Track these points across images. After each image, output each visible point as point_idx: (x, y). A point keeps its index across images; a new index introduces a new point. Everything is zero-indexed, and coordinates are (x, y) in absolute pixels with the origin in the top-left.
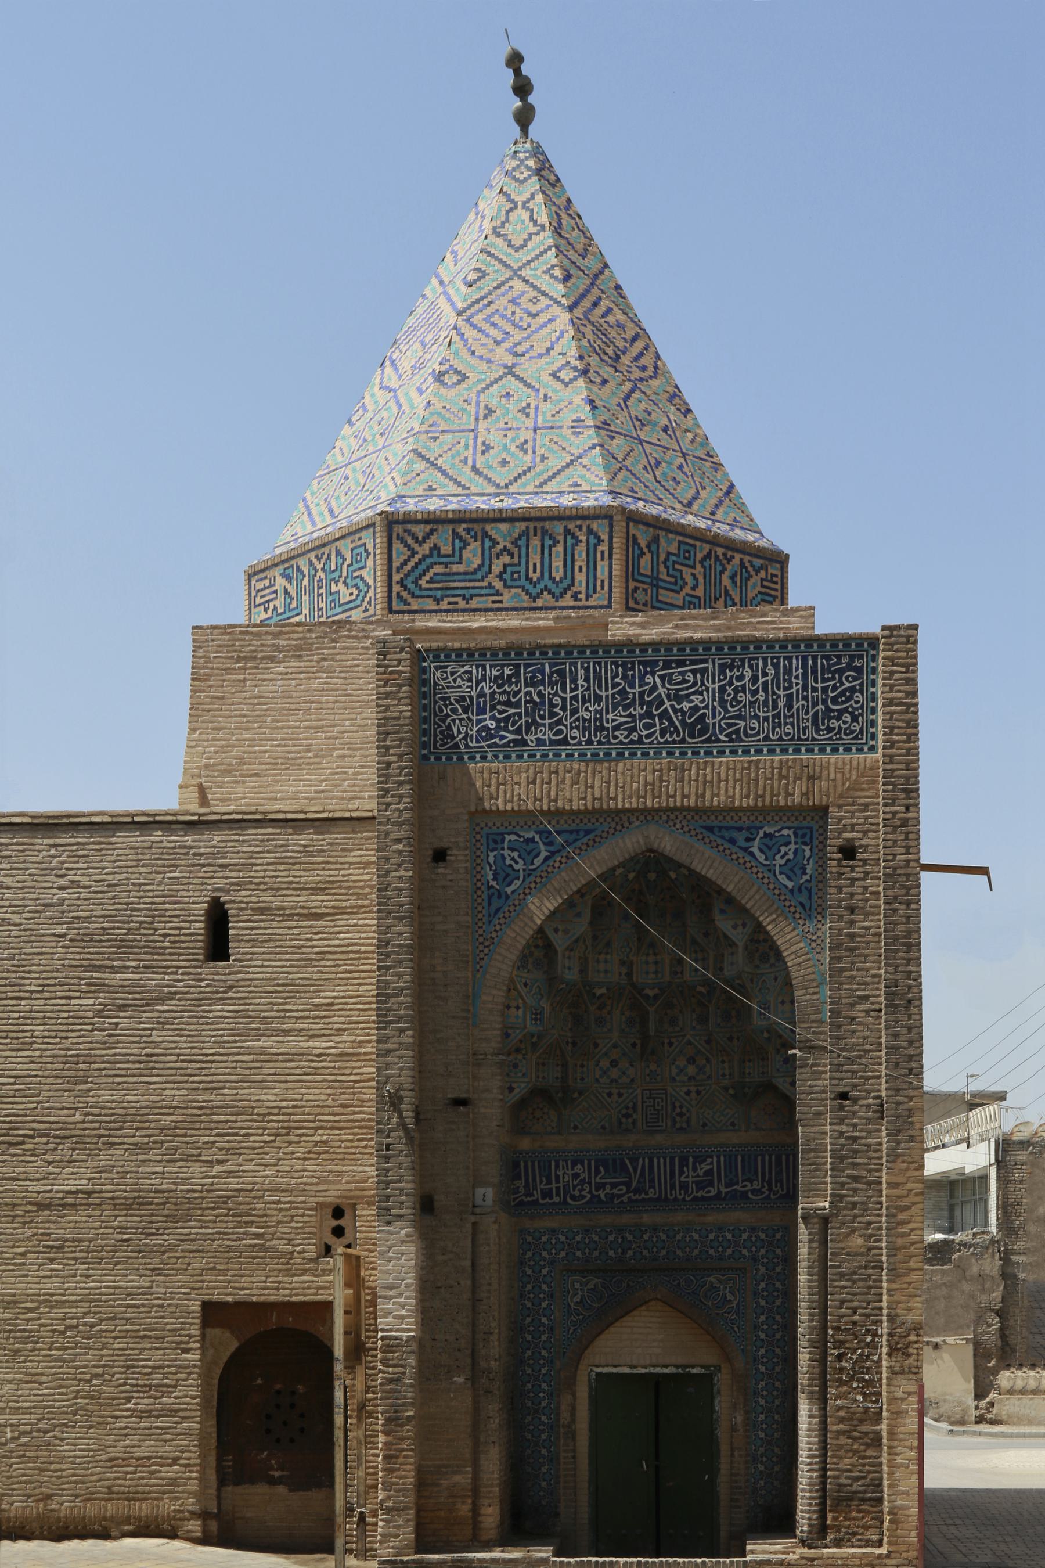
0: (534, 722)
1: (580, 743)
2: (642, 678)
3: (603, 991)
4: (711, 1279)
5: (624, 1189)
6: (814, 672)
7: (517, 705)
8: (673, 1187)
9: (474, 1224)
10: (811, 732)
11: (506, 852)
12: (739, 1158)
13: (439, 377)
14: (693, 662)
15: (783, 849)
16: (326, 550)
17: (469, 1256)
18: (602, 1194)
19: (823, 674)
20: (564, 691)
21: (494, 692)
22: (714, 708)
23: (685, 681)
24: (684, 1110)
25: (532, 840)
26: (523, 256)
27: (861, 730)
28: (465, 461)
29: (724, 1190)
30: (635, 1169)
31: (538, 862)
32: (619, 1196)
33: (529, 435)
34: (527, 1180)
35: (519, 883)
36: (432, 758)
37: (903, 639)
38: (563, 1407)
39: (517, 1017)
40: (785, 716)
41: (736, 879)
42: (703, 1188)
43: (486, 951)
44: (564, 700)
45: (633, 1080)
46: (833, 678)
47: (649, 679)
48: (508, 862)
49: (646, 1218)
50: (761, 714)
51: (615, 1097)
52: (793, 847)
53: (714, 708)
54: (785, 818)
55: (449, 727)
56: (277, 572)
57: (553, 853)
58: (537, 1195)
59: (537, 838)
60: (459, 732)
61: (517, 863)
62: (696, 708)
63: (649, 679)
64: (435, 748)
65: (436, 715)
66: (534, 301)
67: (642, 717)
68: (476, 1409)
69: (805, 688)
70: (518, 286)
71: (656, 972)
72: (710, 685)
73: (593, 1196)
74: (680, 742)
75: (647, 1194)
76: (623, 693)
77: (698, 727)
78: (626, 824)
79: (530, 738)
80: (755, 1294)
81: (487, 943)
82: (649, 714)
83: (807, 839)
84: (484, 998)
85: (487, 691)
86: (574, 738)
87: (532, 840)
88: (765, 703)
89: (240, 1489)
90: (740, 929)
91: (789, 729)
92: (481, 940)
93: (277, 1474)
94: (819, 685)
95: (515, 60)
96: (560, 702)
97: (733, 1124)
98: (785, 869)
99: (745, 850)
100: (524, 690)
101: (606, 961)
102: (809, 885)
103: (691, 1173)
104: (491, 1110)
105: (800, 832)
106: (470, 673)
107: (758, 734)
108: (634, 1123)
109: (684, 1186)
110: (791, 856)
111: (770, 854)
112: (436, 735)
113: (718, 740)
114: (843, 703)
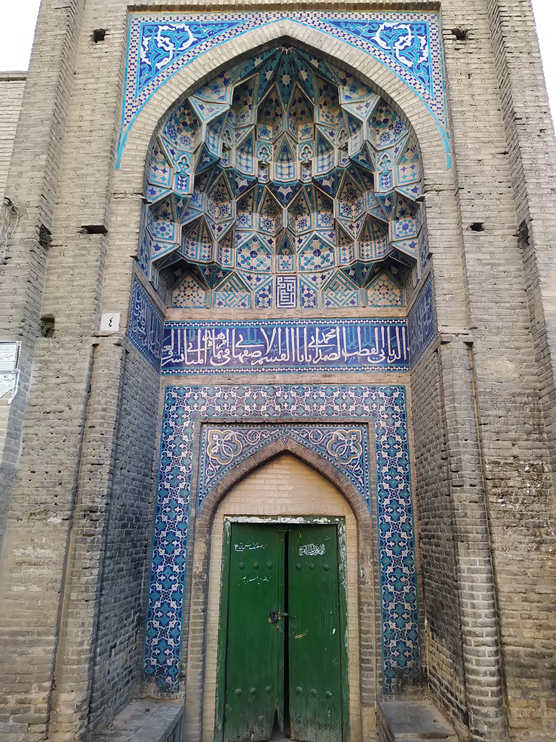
4: (337, 433)
5: (260, 353)
8: (302, 352)
9: (95, 346)
12: (359, 329)
15: (402, 39)
17: (85, 379)
18: (241, 358)
24: (311, 292)
25: (183, 30)
29: (346, 355)
30: (270, 337)
31: (186, 45)
34: (176, 345)
35: (168, 60)
38: (196, 556)
39: (164, 179)
41: (362, 59)
42: (328, 354)
43: (134, 110)
45: (269, 268)
48: (160, 44)
51: (254, 281)
52: (410, 37)
54: (402, 17)
57: (200, 39)
59: (187, 28)
61: (167, 45)
71: (289, 174)
73: (233, 359)
78: (265, 20)
80: (378, 446)
81: (135, 104)
84: (128, 146)
87: (183, 30)
90: (364, 109)
92: (130, 101)
97: (353, 302)
98: (406, 53)
99: (369, 38)
101: (247, 160)
102: (427, 65)
103: (318, 341)
108: (269, 302)
109: (312, 352)
110: (409, 43)
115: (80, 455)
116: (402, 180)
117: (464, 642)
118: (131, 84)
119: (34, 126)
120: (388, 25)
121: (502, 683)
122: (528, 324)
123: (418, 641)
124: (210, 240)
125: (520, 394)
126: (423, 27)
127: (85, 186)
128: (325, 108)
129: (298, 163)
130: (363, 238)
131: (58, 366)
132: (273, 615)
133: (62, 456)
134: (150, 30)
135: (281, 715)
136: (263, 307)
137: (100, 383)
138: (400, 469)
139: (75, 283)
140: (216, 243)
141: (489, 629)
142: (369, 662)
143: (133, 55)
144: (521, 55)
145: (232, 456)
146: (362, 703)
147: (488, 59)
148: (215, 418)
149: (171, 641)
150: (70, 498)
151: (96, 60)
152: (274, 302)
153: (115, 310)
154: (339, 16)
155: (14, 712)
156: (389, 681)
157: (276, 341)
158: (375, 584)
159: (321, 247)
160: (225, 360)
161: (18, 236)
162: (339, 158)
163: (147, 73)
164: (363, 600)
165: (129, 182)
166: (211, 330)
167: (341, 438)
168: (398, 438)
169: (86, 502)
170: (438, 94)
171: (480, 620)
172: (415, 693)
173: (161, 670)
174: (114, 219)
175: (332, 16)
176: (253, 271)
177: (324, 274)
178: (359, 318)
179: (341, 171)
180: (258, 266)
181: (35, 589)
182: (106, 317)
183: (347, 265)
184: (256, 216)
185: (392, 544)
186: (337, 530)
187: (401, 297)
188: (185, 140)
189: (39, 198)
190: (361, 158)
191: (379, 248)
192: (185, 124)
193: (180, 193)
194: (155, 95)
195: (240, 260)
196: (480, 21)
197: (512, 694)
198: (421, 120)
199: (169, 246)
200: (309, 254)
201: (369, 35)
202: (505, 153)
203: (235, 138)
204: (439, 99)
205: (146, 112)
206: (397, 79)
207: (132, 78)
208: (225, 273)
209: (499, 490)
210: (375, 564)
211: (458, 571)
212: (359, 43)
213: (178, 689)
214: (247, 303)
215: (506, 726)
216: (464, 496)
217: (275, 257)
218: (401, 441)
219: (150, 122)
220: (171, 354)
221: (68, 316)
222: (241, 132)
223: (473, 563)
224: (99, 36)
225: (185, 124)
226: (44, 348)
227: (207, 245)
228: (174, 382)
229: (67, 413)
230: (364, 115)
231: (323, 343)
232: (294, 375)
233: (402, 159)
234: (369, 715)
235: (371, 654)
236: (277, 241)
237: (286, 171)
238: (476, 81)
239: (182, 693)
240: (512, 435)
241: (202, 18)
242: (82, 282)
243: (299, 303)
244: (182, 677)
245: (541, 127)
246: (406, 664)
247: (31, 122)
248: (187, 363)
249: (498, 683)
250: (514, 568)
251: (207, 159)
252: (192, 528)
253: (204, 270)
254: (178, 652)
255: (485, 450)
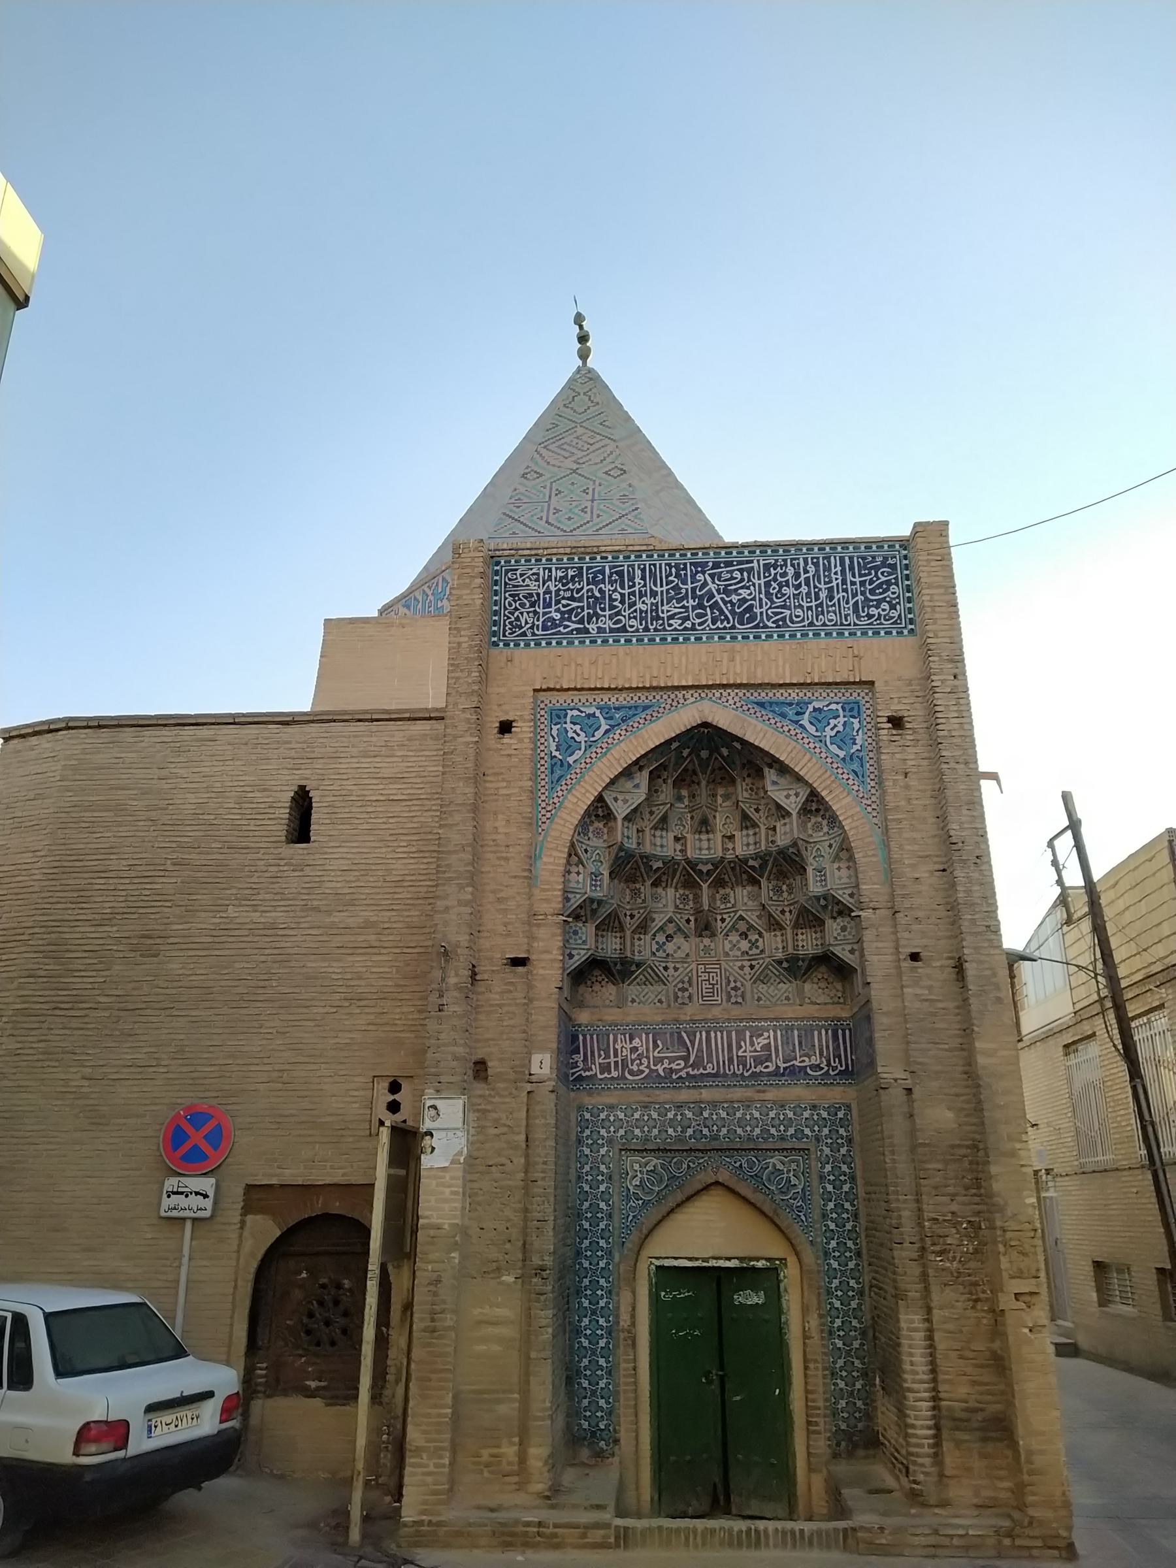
0: (596, 614)
1: (637, 630)
2: (693, 576)
3: (660, 864)
5: (682, 1063)
6: (852, 568)
7: (580, 600)
8: (731, 1060)
10: (852, 618)
11: (569, 726)
13: (524, 476)
14: (740, 563)
16: (435, 580)
17: (523, 1129)
19: (859, 571)
20: (623, 588)
21: (559, 590)
22: (760, 600)
23: (732, 578)
24: (739, 984)
25: (594, 715)
26: (584, 417)
27: (900, 615)
28: (541, 518)
31: (598, 734)
32: (677, 1071)
33: (589, 504)
36: (501, 644)
37: (931, 538)
38: (622, 1309)
39: (578, 882)
40: (828, 606)
41: (789, 749)
43: (548, 815)
44: (622, 595)
45: (687, 955)
46: (870, 574)
47: (700, 577)
48: (571, 734)
49: (706, 1094)
50: (805, 605)
51: (671, 971)
52: (842, 720)
53: (760, 600)
55: (518, 619)
56: (400, 605)
57: (613, 726)
58: (596, 1069)
59: (598, 714)
60: (527, 623)
62: (744, 600)
63: (700, 577)
64: (504, 635)
65: (505, 609)
66: (592, 437)
67: (694, 608)
68: (529, 1316)
69: (844, 582)
70: (580, 431)
71: (709, 849)
72: (756, 582)
73: (651, 1070)
74: (730, 628)
75: (705, 1069)
76: (676, 588)
77: (746, 614)
78: (682, 701)
79: (592, 627)
81: (549, 808)
82: (701, 606)
83: (855, 713)
84: (545, 859)
85: (553, 589)
86: (632, 627)
87: (594, 715)
88: (808, 594)
89: (270, 1402)
90: (793, 798)
91: (832, 616)
92: (543, 805)
93: (313, 1384)
94: (857, 580)
95: (579, 319)
96: (619, 597)
97: (787, 998)
99: (796, 722)
100: (586, 588)
101: (662, 837)
102: (861, 754)
103: (749, 1048)
104: (549, 972)
105: (847, 707)
106: (538, 574)
107: (803, 620)
108: (690, 997)
109: (742, 1061)
110: (840, 728)
111: (819, 725)
112: (505, 625)
113: (767, 627)
114: (881, 594)
115: (526, 1210)
116: (838, 881)
117: (905, 1398)
118: (543, 783)
119: (455, 852)
120: (817, 705)
121: (937, 1436)
122: (966, 1068)
123: (869, 1400)
124: (622, 929)
125: (959, 1146)
126: (856, 706)
127: (505, 911)
128: (748, 780)
129: (719, 835)
130: (796, 925)
131: (494, 1115)
132: (707, 1374)
133: (508, 1212)
134: (558, 715)
135: (720, 1487)
136: (683, 1004)
137: (539, 1135)
138: (847, 1205)
139: (505, 1024)
140: (628, 933)
141: (926, 1385)
142: (817, 1424)
143: (542, 748)
144: (957, 766)
145: (657, 1189)
146: (811, 1469)
147: (926, 755)
148: (635, 1144)
149: (602, 1402)
150: (520, 1256)
151: (505, 759)
152: (695, 998)
153: (542, 1050)
154: (763, 694)
155: (487, 1466)
156: (838, 1445)
157: (700, 1050)
158: (823, 1338)
159: (748, 930)
160: (643, 1072)
161: (452, 980)
162: (767, 839)
163: (559, 768)
164: (809, 1357)
165: (547, 900)
166: (624, 1035)
167: (780, 1166)
168: (844, 1168)
169: (536, 1261)
170: (873, 791)
171: (918, 1377)
172: (866, 1457)
173: (593, 1434)
174: (535, 944)
175: (756, 694)
176: (670, 959)
177: (753, 963)
178: (797, 1019)
179: (770, 854)
180: (675, 952)
181: (496, 1348)
182: (536, 1058)
183: (780, 955)
184: (671, 891)
185: (839, 1293)
186: (778, 1275)
187: (844, 992)
188: (598, 834)
189: (467, 937)
190: (791, 850)
191: (816, 939)
192: (597, 816)
193: (594, 895)
194: (569, 797)
195: (655, 947)
196: (917, 706)
197: (946, 1446)
198: (854, 825)
199: (583, 952)
200: (734, 937)
201: (796, 718)
202: (944, 870)
203: (648, 816)
204: (874, 798)
205: (562, 819)
206: (829, 773)
207: (543, 776)
208: (638, 965)
209: (938, 1248)
210: (821, 1316)
211: (899, 1329)
212: (786, 729)
213: (613, 1455)
214: (664, 999)
215: (941, 1475)
216: (904, 1254)
217: (694, 940)
218: (847, 1171)
219: (566, 830)
220: (581, 1065)
221: (501, 1060)
222: (654, 809)
223: (912, 1322)
224: (506, 728)
225: (597, 816)
226: (480, 1096)
227: (618, 935)
228: (588, 1101)
229: (509, 1167)
230: (793, 806)
231: (756, 1051)
232: (723, 1090)
233: (837, 858)
234: (818, 1482)
235: (818, 1415)
236: (696, 920)
237: (705, 844)
238: (913, 782)
239: (616, 1459)
240: (951, 1189)
241: (613, 700)
242: (511, 1022)
243: (724, 998)
244: (617, 1441)
245: (978, 853)
246: (856, 1426)
247: (451, 848)
248: (600, 1076)
249: (935, 1436)
250: (950, 1326)
251: (623, 854)
252: (616, 1275)
253: (616, 965)
254: (610, 1413)
255: (925, 1206)
